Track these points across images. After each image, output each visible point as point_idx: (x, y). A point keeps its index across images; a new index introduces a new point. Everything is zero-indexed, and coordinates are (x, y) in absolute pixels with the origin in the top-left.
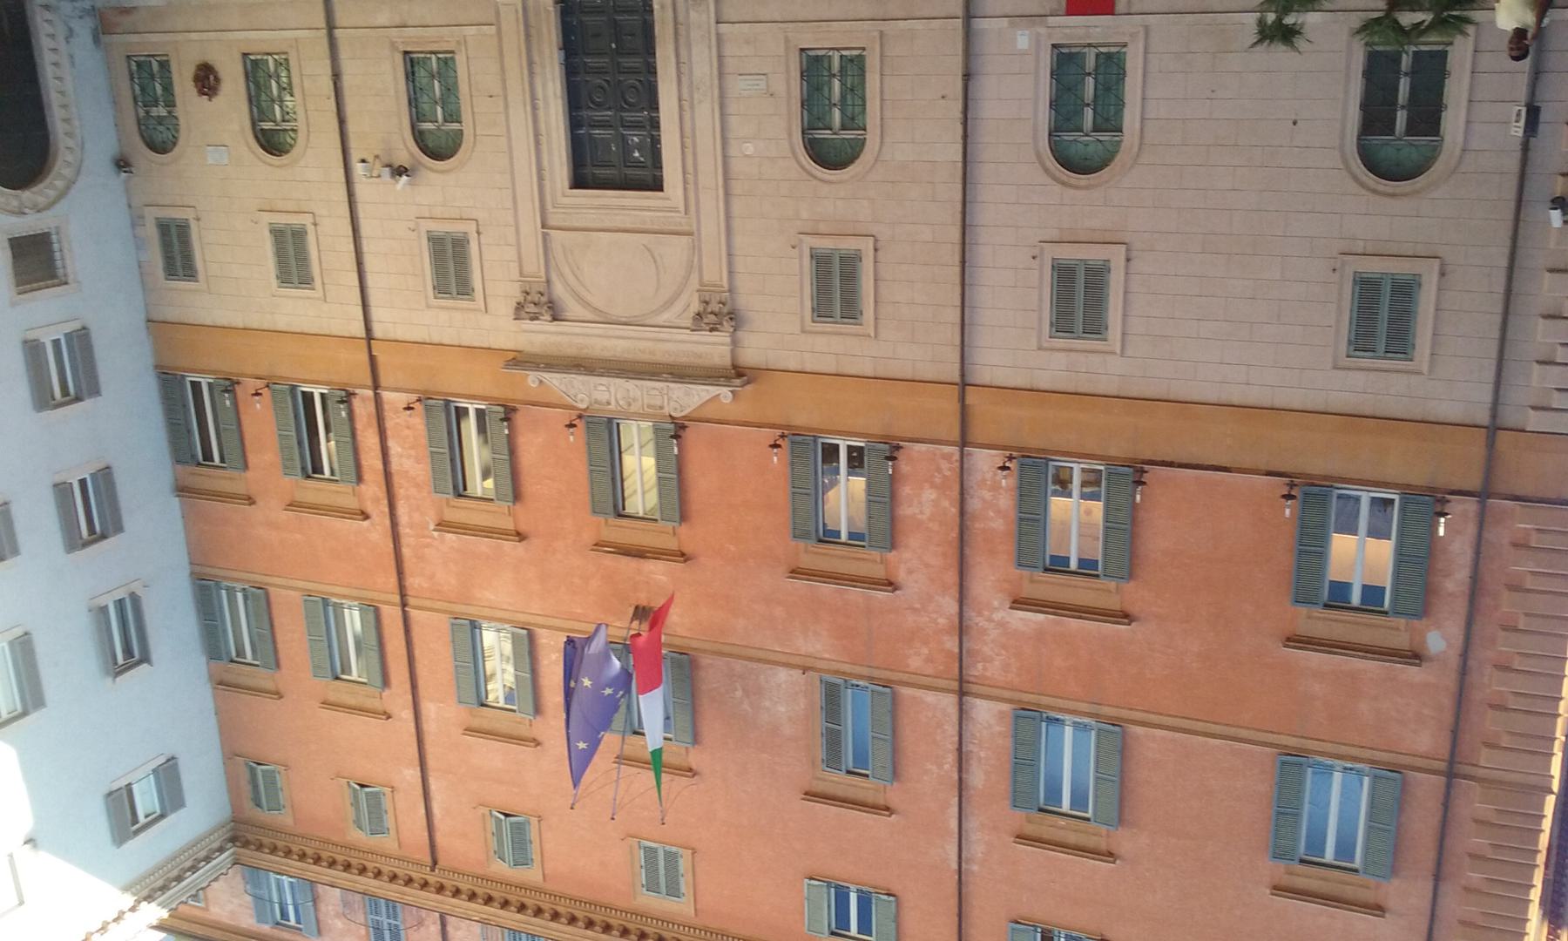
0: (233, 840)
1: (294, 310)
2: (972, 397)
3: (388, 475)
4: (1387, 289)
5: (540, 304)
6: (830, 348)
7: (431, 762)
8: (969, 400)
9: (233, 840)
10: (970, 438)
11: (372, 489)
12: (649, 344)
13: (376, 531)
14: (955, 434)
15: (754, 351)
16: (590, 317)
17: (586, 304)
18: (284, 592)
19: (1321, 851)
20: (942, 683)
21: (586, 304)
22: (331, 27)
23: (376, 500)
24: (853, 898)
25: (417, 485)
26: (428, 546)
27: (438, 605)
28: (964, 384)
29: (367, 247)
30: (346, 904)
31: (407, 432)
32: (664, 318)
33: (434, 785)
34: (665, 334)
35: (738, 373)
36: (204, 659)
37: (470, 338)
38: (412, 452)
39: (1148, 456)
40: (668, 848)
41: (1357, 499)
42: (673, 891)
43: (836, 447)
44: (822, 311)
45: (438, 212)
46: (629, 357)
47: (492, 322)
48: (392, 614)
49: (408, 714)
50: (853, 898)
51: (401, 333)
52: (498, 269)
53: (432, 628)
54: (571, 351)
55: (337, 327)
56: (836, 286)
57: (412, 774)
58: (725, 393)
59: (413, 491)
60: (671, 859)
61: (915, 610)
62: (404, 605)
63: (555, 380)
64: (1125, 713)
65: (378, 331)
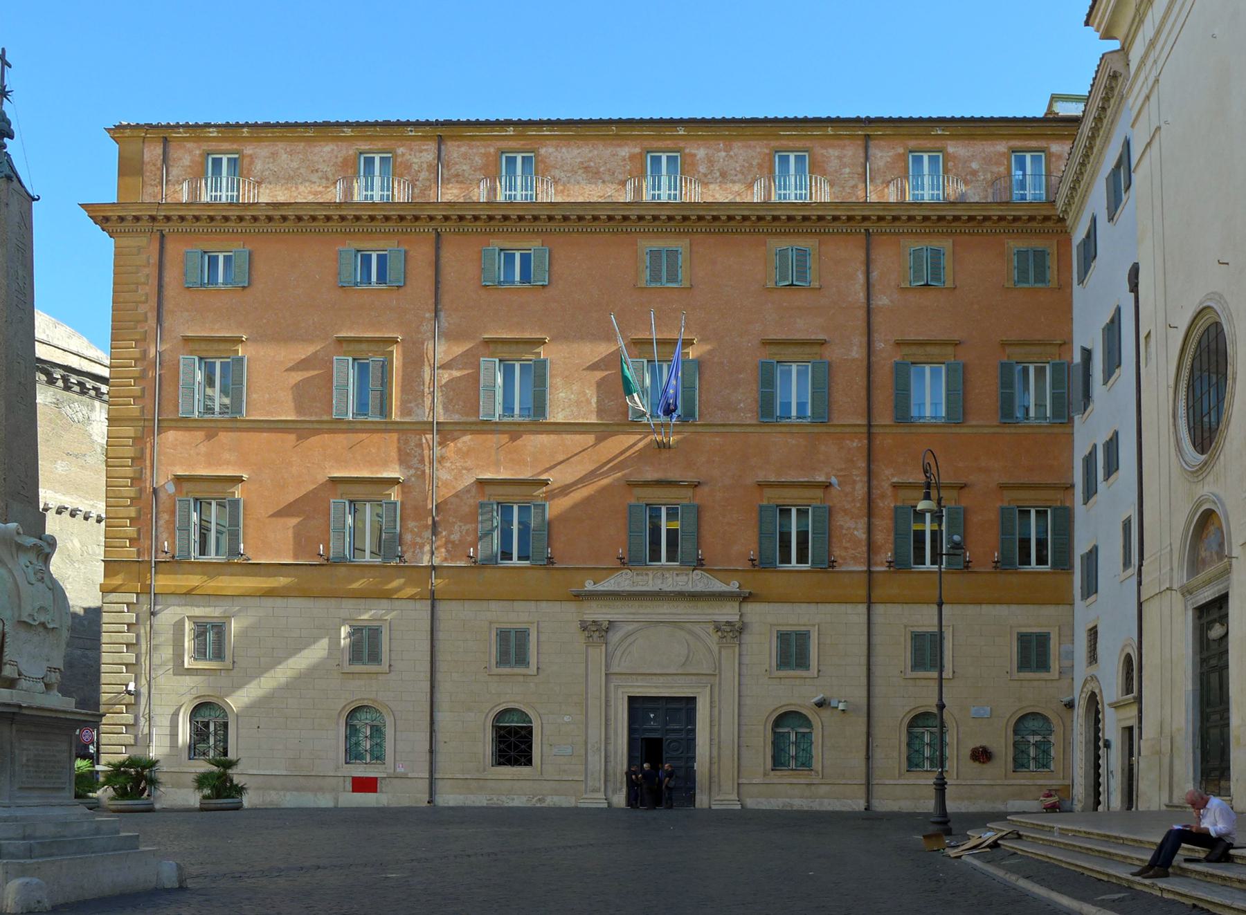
2: (863, 592)
5: (735, 631)
6: (517, 615)
7: (861, 314)
11: (886, 504)
12: (641, 611)
15: (570, 613)
16: (688, 625)
17: (691, 633)
18: (859, 422)
19: (932, 370)
20: (881, 430)
21: (691, 633)
22: (432, 780)
23: (883, 496)
24: (374, 278)
25: (845, 511)
26: (842, 470)
27: (839, 430)
28: (870, 603)
29: (864, 660)
31: (848, 545)
32: (631, 627)
33: (862, 296)
34: (631, 617)
35: (581, 597)
37: (786, 608)
39: (323, 568)
40: (658, 285)
41: (520, 558)
42: (655, 255)
43: (668, 560)
46: (660, 603)
47: (766, 620)
48: (884, 417)
50: (374, 278)
51: (849, 608)
52: (761, 647)
53: (849, 414)
54: (700, 604)
55: (958, 609)
56: (513, 648)
57: (882, 300)
58: (589, 586)
60: (656, 277)
61: (466, 469)
62: (869, 426)
63: (717, 586)
64: (758, 429)
65: (862, 608)
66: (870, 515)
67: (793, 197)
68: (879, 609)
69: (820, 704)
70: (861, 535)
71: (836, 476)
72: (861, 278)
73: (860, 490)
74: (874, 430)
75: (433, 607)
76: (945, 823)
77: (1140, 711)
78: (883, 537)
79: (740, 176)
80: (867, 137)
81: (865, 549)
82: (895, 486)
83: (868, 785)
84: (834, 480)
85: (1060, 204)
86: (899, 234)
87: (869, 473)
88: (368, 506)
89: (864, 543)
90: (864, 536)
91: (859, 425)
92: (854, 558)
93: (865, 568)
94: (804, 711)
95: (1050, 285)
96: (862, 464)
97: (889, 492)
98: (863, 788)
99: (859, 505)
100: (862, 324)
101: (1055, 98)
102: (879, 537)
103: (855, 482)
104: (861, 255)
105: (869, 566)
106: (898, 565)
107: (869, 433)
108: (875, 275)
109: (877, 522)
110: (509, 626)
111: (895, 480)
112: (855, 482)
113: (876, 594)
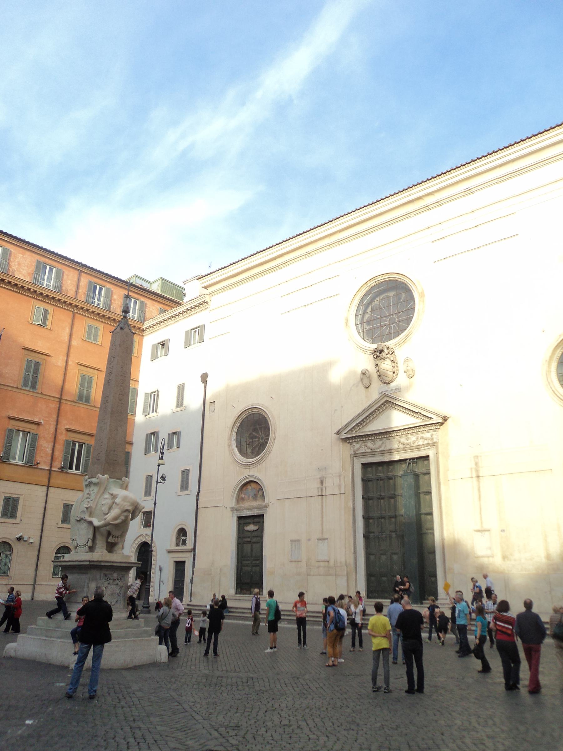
0: (144, 331)
1: (72, 497)
2: (46, 481)
3: (55, 442)
4: (9, 514)
7: (65, 346)
8: (47, 481)
9: (144, 331)
10: (48, 472)
11: (63, 437)
13: (65, 424)
14: (52, 472)
25: (44, 437)
26: (46, 417)
27: (47, 397)
28: (48, 486)
30: (67, 293)
33: (66, 338)
36: (139, 389)
38: (42, 448)
43: (76, 470)
44: (16, 500)
45: (10, 525)
49: (70, 363)
57: (74, 343)
59: (46, 436)
65: (45, 489)
66: (55, 442)
67: (45, 285)
68: (51, 490)
69: (19, 539)
70: (49, 451)
71: (43, 420)
72: (67, 330)
73: (52, 429)
74: (62, 401)
75: (48, 489)
76: (148, 607)
77: (194, 555)
78: (59, 454)
79: (26, 268)
80: (81, 271)
81: (50, 458)
82: (68, 430)
83: (34, 585)
84: (42, 421)
85: (146, 325)
86: (85, 316)
87: (57, 421)
88: (21, 433)
89: (50, 455)
90: (51, 452)
91: (56, 398)
92: (45, 462)
93: (49, 468)
94: (10, 542)
95: (98, 343)
96: (55, 416)
97: (64, 432)
98: (31, 587)
99: (50, 436)
100: (65, 351)
101: (136, 276)
102: (57, 453)
103: (50, 424)
104: (70, 320)
105: (51, 467)
106: (62, 469)
107: (60, 402)
108: (74, 330)
109: (57, 446)
110: (10, 495)
111: (67, 427)
112: (50, 424)
113: (52, 481)
